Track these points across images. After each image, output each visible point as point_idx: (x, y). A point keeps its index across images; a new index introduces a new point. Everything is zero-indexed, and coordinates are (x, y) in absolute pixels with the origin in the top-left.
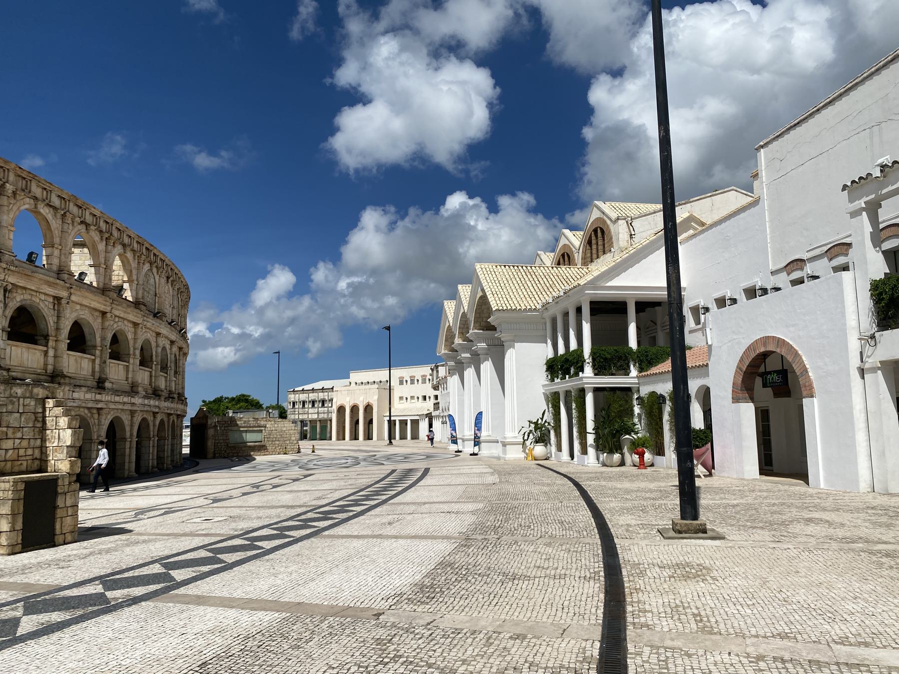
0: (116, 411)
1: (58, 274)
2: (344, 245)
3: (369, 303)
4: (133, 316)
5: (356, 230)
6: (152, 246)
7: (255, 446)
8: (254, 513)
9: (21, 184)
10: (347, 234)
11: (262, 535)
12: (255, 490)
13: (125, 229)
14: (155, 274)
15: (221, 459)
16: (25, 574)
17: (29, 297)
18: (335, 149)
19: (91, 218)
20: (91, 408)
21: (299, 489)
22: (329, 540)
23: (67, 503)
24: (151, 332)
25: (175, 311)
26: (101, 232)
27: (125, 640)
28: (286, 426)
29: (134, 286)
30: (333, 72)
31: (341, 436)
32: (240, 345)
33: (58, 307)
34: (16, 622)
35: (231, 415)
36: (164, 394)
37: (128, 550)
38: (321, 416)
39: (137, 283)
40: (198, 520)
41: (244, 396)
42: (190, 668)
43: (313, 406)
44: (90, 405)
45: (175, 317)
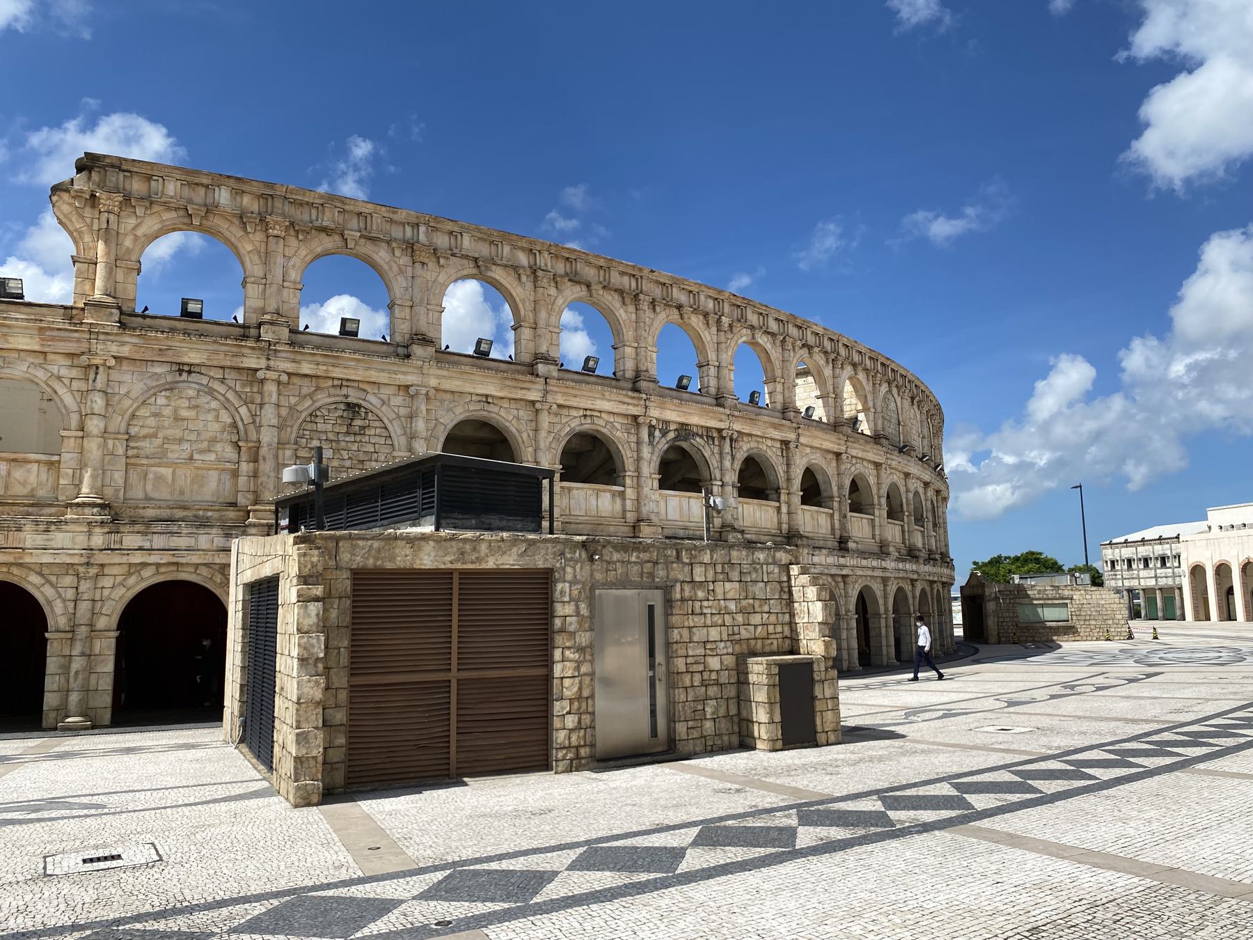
0: (864, 578)
1: (716, 399)
2: (1175, 304)
3: (1231, 392)
4: (874, 453)
5: (1194, 277)
6: (888, 359)
7: (1058, 627)
8: (1074, 726)
9: (737, 313)
10: (1180, 286)
11: (1091, 758)
12: (1068, 691)
13: (854, 344)
14: (896, 395)
15: (1009, 645)
16: (792, 776)
17: (756, 445)
18: (1146, 158)
19: (756, 316)
20: (835, 575)
21: (1141, 695)
22: (1208, 779)
23: (826, 693)
24: (898, 473)
25: (926, 442)
26: (826, 353)
27: (922, 877)
28: (1102, 597)
29: (871, 415)
30: (1130, 39)
31: (1202, 613)
32: (1019, 480)
33: (787, 453)
34: (678, 854)
35: (1017, 581)
36: (922, 555)
37: (904, 760)
38: (1162, 582)
39: (874, 411)
40: (991, 729)
41: (1032, 553)
42: (1015, 931)
43: (1146, 566)
44: (833, 571)
45: (926, 450)
